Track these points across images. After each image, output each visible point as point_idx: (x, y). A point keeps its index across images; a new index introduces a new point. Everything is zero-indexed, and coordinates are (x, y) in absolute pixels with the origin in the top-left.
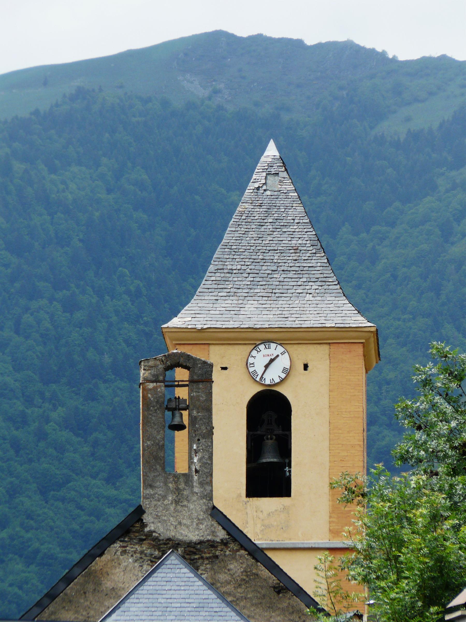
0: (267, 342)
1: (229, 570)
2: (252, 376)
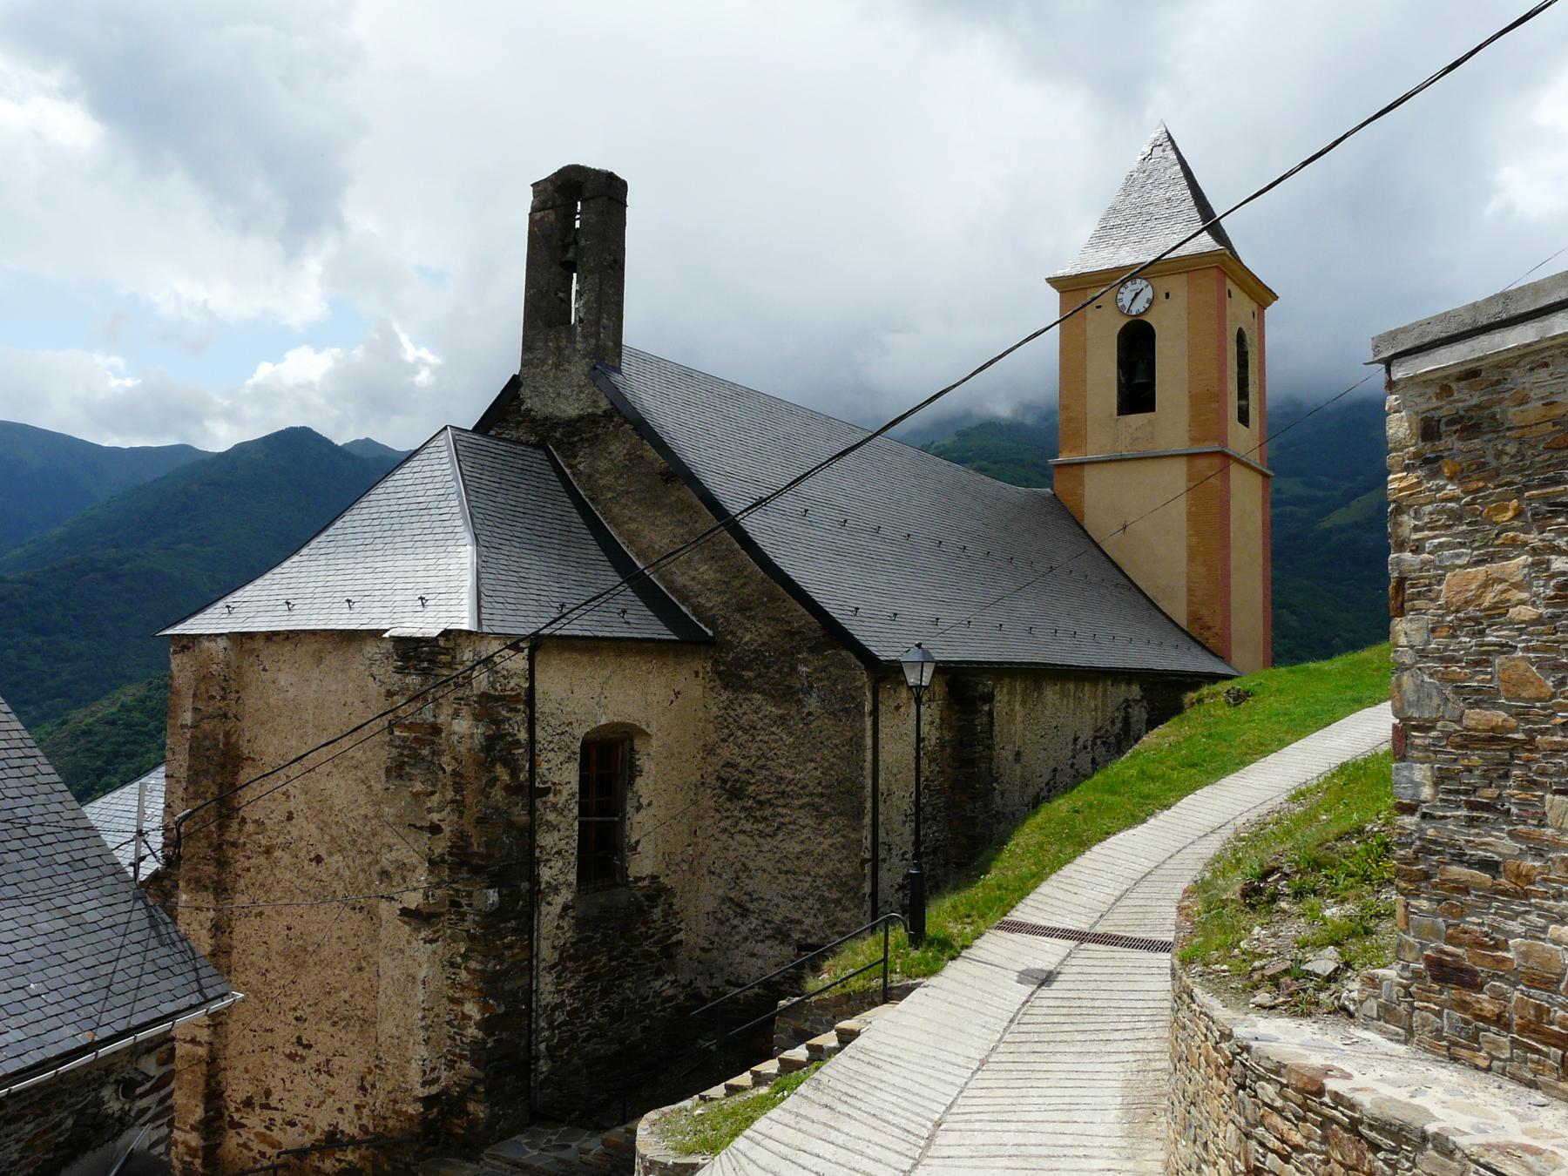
0: (1133, 277)
1: (610, 454)
2: (1120, 310)
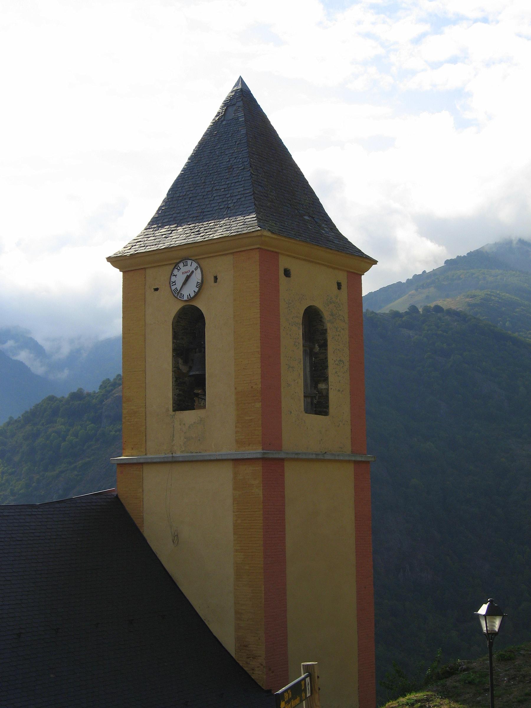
0: (184, 260)
